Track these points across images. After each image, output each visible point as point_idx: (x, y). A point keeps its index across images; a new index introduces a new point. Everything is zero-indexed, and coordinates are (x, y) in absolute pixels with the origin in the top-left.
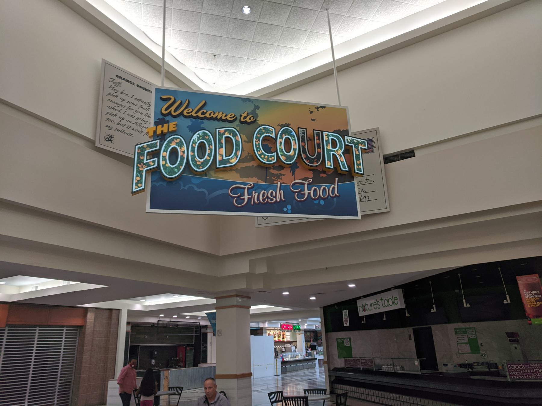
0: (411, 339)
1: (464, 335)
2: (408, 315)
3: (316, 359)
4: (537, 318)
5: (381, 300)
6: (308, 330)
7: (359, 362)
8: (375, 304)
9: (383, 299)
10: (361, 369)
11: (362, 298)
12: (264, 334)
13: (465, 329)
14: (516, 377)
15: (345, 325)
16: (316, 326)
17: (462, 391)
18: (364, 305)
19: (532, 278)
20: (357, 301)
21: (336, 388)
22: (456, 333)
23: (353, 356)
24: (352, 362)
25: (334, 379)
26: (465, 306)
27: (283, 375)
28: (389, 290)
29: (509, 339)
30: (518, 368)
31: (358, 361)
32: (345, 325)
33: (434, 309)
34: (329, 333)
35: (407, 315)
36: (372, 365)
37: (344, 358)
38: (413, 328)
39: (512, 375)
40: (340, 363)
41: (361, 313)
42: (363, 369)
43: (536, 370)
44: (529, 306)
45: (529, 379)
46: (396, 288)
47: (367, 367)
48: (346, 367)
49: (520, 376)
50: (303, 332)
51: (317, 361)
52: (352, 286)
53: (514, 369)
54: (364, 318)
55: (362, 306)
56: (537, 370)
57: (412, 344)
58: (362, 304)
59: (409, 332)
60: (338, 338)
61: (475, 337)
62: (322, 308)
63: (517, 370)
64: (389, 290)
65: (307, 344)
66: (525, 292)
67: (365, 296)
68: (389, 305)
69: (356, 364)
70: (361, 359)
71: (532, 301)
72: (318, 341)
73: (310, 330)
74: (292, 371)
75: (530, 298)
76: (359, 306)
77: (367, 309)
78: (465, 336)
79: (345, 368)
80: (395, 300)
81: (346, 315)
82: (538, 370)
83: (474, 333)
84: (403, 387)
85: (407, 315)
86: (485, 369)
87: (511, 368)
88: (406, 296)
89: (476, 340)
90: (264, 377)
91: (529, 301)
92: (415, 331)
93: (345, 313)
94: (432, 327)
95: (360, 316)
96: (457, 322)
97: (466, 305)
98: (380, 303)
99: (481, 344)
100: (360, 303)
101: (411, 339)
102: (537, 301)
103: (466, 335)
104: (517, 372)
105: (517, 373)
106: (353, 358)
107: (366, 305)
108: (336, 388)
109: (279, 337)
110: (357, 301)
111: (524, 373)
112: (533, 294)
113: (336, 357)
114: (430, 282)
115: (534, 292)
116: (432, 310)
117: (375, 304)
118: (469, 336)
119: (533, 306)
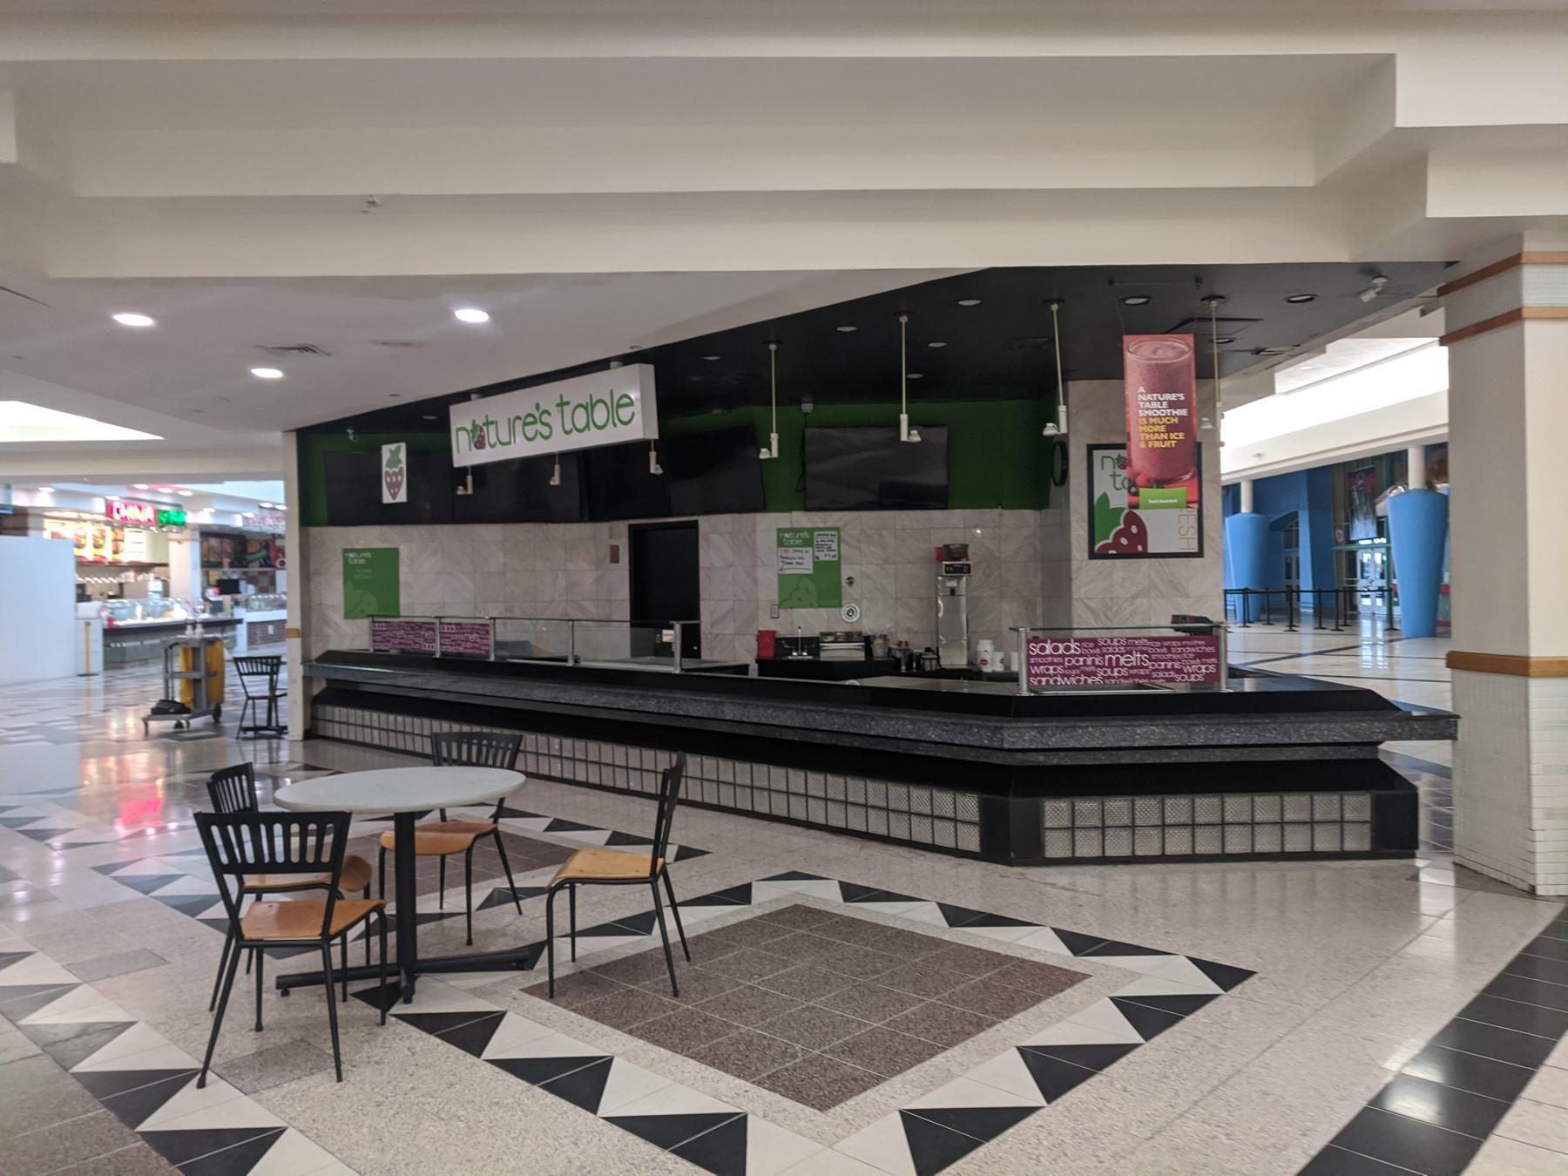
0: (617, 562)
1: (804, 549)
2: (657, 469)
3: (240, 621)
4: (1158, 487)
5: (558, 405)
6: (216, 528)
7: (428, 634)
8: (530, 419)
9: (568, 403)
10: (438, 655)
11: (473, 396)
12: (31, 532)
13: (811, 531)
14: (1048, 681)
15: (387, 498)
16: (246, 519)
17: (656, 711)
18: (479, 423)
19: (1174, 348)
20: (453, 408)
21: (329, 721)
22: (780, 544)
23: (402, 614)
24: (400, 633)
25: (324, 690)
26: (904, 437)
27: (111, 673)
28: (602, 365)
29: (947, 565)
30: (1060, 652)
31: (428, 629)
32: (387, 498)
33: (770, 449)
34: (315, 528)
35: (655, 468)
36: (485, 641)
37: (369, 616)
38: (630, 526)
39: (1036, 675)
40: (352, 635)
41: (465, 455)
42: (443, 654)
43: (1110, 659)
44: (1143, 445)
45: (1086, 686)
46: (627, 359)
47: (461, 649)
48: (375, 650)
49: (1059, 679)
50: (197, 535)
51: (242, 630)
52: (472, 316)
53: (1047, 656)
54: (469, 478)
55: (469, 428)
56: (1114, 657)
57: (620, 576)
58: (474, 422)
59: (611, 536)
60: (349, 547)
61: (836, 559)
62: (294, 435)
63: (1055, 660)
64: (602, 365)
65: (206, 575)
66: (1141, 393)
67: (487, 391)
68: (591, 425)
69: (417, 640)
70: (441, 623)
71: (1157, 428)
72: (247, 567)
73: (221, 531)
74: (146, 660)
75: (1153, 417)
76: (458, 430)
77: (493, 440)
78: (807, 552)
79: (372, 650)
80: (619, 406)
81: (394, 461)
82: (1118, 659)
83: (835, 546)
84: (487, 702)
85: (655, 468)
86: (855, 653)
87: (1037, 651)
88: (668, 402)
89: (835, 567)
90: (25, 683)
91: (1145, 428)
92: (636, 535)
93: (395, 453)
94: (700, 522)
95: (456, 464)
96: (790, 510)
97: (909, 434)
98: (554, 420)
99: (850, 578)
100: (461, 418)
101: (617, 562)
102: (1170, 428)
103: (810, 549)
104: (1052, 664)
105: (1051, 668)
106: (401, 619)
107: (492, 423)
108: (329, 721)
109: (97, 546)
110: (453, 408)
111: (1074, 667)
112: (1165, 404)
113: (337, 616)
114: (773, 347)
115: (1168, 396)
116: (763, 450)
117: (530, 419)
118: (817, 554)
119: (1157, 444)
